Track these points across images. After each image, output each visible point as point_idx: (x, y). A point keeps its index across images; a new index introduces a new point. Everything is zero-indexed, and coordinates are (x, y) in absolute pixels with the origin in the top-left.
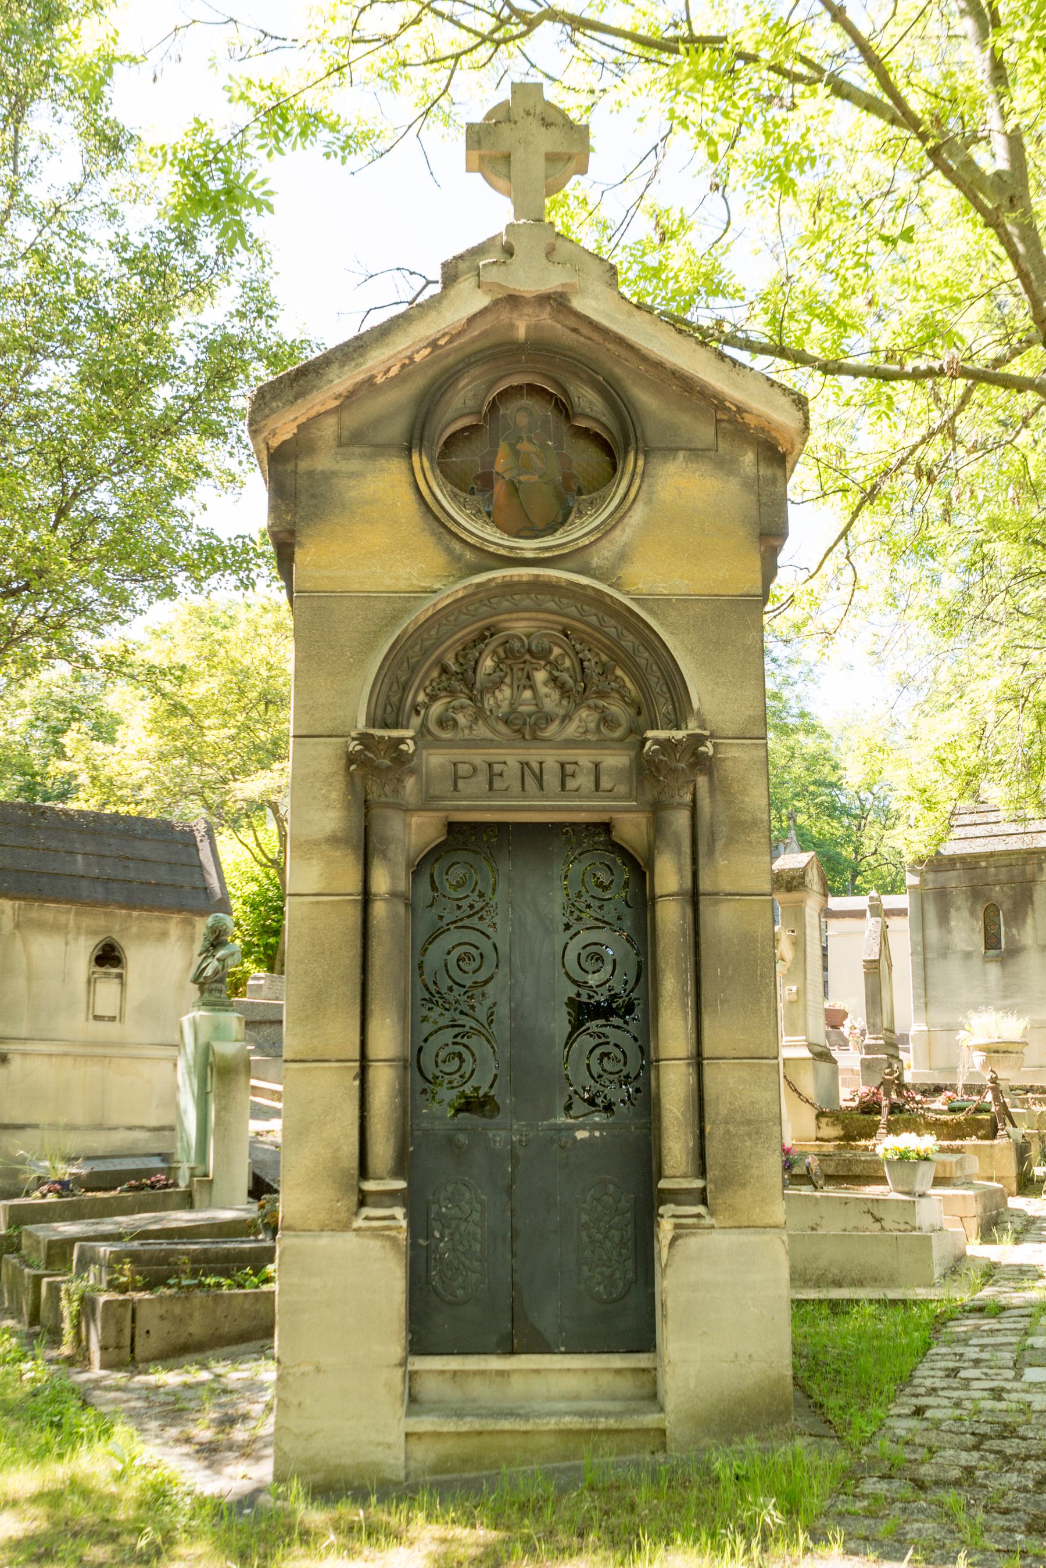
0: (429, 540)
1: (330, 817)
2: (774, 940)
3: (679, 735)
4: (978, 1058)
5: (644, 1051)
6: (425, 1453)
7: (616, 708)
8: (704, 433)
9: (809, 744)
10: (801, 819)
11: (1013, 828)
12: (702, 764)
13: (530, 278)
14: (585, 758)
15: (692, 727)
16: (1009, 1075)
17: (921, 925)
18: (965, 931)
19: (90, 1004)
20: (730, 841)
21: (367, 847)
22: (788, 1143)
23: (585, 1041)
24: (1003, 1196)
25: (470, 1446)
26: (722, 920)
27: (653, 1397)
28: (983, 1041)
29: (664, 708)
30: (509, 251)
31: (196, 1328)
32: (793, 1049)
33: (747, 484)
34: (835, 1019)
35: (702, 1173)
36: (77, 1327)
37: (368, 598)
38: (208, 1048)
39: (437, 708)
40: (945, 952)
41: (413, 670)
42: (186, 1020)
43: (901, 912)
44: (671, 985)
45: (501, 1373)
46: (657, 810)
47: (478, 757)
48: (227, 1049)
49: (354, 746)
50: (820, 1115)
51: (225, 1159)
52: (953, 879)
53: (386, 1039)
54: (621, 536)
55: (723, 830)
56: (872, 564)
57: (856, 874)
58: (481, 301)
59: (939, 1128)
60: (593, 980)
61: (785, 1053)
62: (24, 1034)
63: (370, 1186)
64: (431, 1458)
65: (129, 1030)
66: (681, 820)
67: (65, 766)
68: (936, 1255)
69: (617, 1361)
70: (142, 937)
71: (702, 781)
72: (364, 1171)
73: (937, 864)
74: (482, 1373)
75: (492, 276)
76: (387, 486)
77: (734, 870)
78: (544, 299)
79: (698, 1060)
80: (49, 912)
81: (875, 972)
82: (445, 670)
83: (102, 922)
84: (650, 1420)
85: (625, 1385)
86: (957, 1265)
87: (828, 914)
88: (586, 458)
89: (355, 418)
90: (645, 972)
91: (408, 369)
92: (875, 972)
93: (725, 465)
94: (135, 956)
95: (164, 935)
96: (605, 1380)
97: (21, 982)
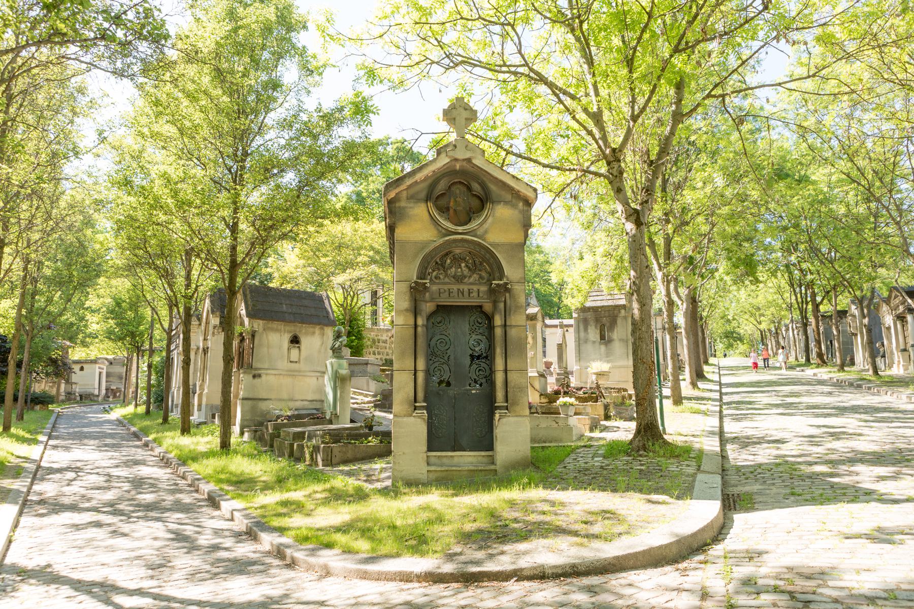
0: (432, 227)
1: (406, 304)
2: (527, 337)
3: (501, 282)
4: (594, 377)
5: (491, 369)
6: (433, 476)
7: (484, 274)
8: (508, 197)
9: (541, 257)
10: (537, 285)
11: (609, 297)
12: (508, 290)
13: (461, 154)
14: (475, 288)
15: (505, 280)
16: (603, 383)
17: (578, 331)
18: (593, 334)
19: (289, 357)
20: (515, 311)
21: (416, 312)
22: (530, 401)
23: (475, 366)
24: (599, 421)
25: (444, 474)
26: (513, 333)
27: (493, 463)
28: (595, 371)
29: (497, 275)
30: (455, 146)
31: (350, 455)
32: (532, 373)
33: (520, 212)
34: (548, 365)
35: (507, 401)
36: (312, 456)
37: (416, 243)
38: (337, 371)
39: (435, 274)
40: (586, 341)
41: (429, 263)
42: (328, 362)
43: (571, 326)
44: (499, 351)
45: (452, 456)
46: (495, 303)
47: (446, 287)
48: (344, 372)
49: (413, 285)
50: (541, 395)
51: (342, 408)
52: (589, 315)
53: (421, 365)
54: (486, 226)
55: (513, 308)
56: (560, 214)
57: (559, 308)
58: (447, 160)
59: (577, 398)
60: (477, 349)
61: (530, 374)
62: (266, 367)
63: (417, 404)
64: (434, 477)
65: (302, 366)
66: (502, 305)
67: (269, 270)
68: (574, 433)
69: (483, 453)
70: (306, 334)
71: (507, 295)
72: (415, 401)
73: (584, 310)
74: (446, 456)
75: (451, 154)
76: (420, 211)
77: (517, 319)
78: (464, 160)
79: (506, 371)
80: (275, 325)
81: (561, 348)
82: (437, 263)
83: (293, 328)
84: (493, 467)
85: (485, 460)
86: (581, 437)
87: (547, 326)
88: (475, 203)
89: (412, 191)
90: (491, 347)
91: (426, 178)
92: (561, 348)
93: (514, 206)
94: (305, 341)
95: (314, 333)
96: (480, 458)
97: (266, 349)
